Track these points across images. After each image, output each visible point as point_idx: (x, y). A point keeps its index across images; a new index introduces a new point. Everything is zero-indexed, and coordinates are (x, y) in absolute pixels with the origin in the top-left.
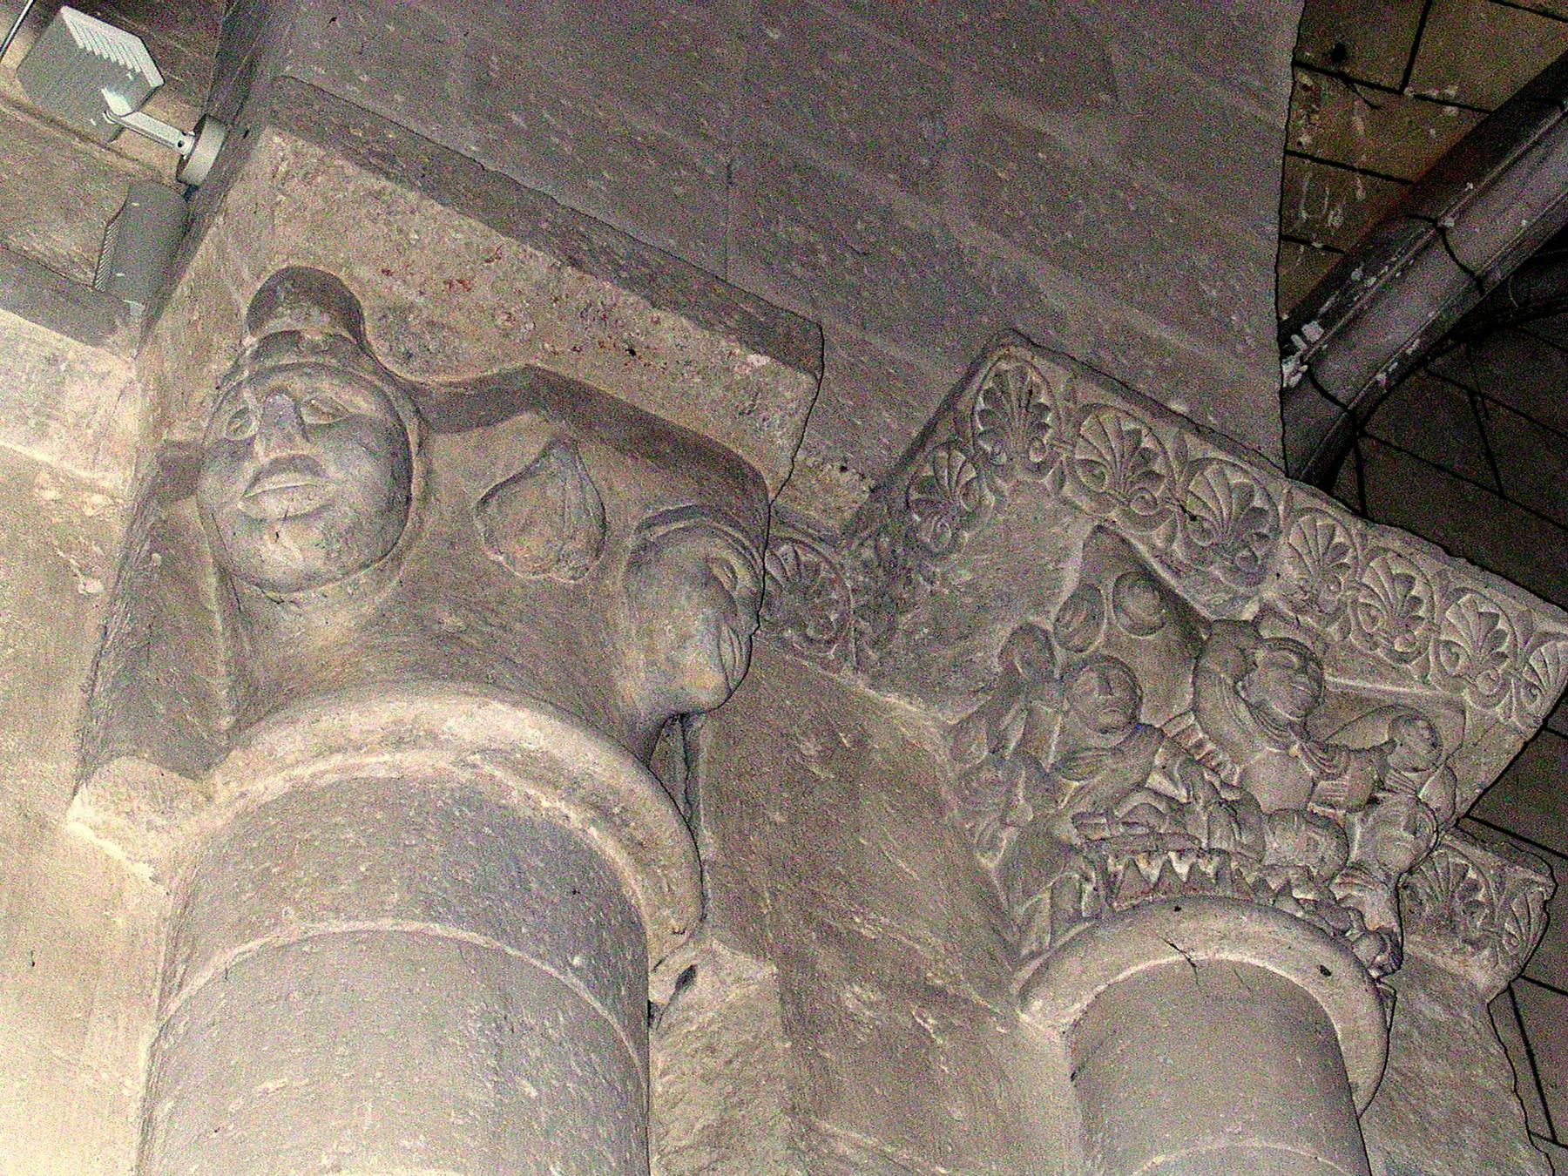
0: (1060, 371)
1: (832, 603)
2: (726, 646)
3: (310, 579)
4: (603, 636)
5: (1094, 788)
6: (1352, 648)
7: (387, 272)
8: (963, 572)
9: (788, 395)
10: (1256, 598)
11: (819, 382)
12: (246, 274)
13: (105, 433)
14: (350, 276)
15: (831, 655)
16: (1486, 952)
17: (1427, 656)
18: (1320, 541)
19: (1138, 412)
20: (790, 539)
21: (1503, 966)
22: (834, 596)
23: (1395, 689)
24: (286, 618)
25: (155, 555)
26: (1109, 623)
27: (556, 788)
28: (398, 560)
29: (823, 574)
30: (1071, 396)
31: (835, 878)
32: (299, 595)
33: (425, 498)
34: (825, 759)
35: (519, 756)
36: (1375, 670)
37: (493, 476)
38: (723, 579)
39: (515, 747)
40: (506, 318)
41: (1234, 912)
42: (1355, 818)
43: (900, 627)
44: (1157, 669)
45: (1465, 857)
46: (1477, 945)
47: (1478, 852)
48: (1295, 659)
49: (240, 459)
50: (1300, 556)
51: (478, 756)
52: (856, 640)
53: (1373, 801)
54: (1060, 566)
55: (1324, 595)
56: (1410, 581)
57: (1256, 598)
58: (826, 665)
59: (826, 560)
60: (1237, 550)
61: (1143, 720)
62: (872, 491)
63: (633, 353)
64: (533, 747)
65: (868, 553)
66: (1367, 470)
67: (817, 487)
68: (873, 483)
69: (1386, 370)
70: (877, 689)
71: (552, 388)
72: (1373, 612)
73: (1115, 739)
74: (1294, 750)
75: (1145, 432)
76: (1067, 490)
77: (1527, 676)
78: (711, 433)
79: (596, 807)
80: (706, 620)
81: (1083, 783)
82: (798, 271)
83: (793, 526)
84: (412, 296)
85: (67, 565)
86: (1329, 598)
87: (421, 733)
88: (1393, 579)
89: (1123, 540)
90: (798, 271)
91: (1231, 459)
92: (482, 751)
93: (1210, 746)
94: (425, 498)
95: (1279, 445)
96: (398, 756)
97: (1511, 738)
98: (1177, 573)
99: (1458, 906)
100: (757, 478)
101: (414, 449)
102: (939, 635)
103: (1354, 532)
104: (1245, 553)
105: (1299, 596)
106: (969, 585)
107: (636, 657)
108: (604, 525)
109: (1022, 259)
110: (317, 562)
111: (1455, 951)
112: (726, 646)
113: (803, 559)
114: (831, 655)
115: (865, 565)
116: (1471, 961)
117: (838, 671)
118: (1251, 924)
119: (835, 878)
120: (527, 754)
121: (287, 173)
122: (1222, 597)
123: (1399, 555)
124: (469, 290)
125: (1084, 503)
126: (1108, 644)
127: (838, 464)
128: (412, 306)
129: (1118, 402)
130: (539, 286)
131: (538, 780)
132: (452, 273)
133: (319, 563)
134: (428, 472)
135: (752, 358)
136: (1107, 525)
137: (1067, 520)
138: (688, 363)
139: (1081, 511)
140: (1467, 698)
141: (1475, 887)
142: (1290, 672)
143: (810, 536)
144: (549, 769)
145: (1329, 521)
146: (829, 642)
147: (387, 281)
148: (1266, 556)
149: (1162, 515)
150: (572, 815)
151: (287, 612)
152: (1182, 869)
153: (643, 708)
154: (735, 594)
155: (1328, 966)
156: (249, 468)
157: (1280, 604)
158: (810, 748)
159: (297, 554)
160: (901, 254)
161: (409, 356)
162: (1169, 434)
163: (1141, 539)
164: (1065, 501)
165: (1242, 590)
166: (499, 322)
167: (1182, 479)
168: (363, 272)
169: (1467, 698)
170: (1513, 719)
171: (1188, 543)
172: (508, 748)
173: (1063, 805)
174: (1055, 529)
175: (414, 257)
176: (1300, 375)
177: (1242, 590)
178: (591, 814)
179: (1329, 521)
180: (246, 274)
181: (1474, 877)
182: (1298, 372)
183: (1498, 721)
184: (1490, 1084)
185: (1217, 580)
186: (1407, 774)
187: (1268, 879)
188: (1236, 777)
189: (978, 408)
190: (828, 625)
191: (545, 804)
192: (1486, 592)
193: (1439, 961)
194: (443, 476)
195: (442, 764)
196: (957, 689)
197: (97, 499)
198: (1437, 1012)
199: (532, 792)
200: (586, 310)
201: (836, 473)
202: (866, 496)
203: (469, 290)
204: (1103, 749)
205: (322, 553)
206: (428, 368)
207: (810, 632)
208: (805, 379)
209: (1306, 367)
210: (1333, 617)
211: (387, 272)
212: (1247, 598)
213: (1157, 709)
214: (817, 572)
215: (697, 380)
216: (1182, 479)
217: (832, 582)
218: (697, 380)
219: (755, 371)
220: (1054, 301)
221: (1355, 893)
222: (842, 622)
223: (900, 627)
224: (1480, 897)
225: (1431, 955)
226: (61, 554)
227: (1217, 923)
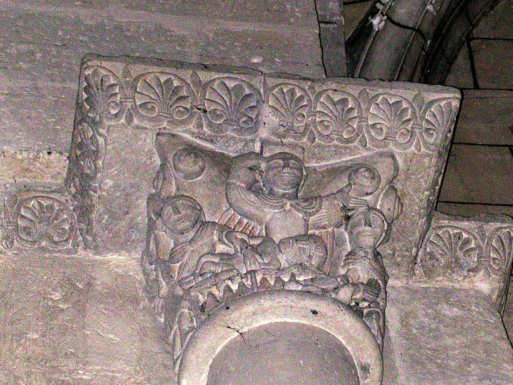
0: (118, 64)
1: (64, 221)
5: (186, 263)
6: (319, 145)
8: (108, 181)
10: (258, 139)
15: (70, 246)
16: (482, 273)
17: (363, 136)
18: (287, 99)
19: (167, 70)
20: (35, 197)
21: (494, 276)
22: (65, 216)
23: (352, 157)
26: (175, 179)
30: (127, 73)
34: (65, 299)
36: (337, 152)
41: (256, 300)
42: (342, 229)
43: (94, 219)
44: (209, 193)
45: (458, 228)
46: (475, 270)
47: (466, 223)
48: (281, 162)
50: (277, 109)
53: (348, 218)
54: (153, 160)
55: (296, 125)
56: (344, 101)
57: (258, 139)
58: (68, 252)
60: (239, 119)
61: (208, 218)
62: (68, 158)
66: (475, 57)
67: (42, 167)
68: (67, 154)
69: (431, 3)
70: (99, 254)
72: (326, 123)
73: (191, 235)
74: (288, 207)
75: (173, 78)
76: (136, 121)
77: (424, 125)
81: (180, 263)
82: (24, 66)
83: (35, 190)
86: (300, 125)
88: (334, 104)
89: (173, 135)
90: (24, 66)
91: (227, 75)
93: (245, 221)
95: (320, 60)
97: (426, 160)
98: (212, 141)
99: (460, 254)
102: (113, 216)
103: (307, 88)
104: (245, 119)
105: (282, 129)
106: (114, 186)
109: (158, 18)
111: (465, 277)
113: (45, 204)
114: (70, 246)
116: (475, 279)
117: (76, 252)
118: (266, 303)
122: (240, 145)
123: (335, 90)
125: (146, 124)
126: (178, 189)
127: (45, 152)
129: (156, 69)
136: (163, 131)
137: (143, 136)
139: (146, 128)
140: (393, 148)
141: (467, 241)
142: (280, 169)
145: (290, 87)
146: (66, 240)
148: (257, 116)
149: (192, 115)
152: (235, 287)
155: (317, 309)
157: (272, 137)
160: (85, 39)
162: (187, 74)
163: (185, 132)
164: (138, 127)
165: (249, 137)
167: (199, 95)
169: (393, 148)
170: (423, 149)
171: (210, 125)
173: (176, 277)
174: (140, 143)
176: (383, 22)
177: (249, 137)
179: (290, 87)
181: (467, 236)
182: (382, 21)
183: (414, 154)
184: (489, 338)
185: (233, 138)
186: (364, 198)
187: (282, 276)
188: (264, 231)
189: (84, 98)
192: (393, 92)
193: (457, 286)
196: (139, 240)
198: (456, 311)
201: (47, 156)
204: (184, 243)
209: (386, 17)
210: (303, 134)
212: (253, 141)
213: (214, 213)
216: (199, 95)
220: (179, 32)
221: (351, 267)
223: (94, 219)
224: (473, 245)
225: (451, 284)
227: (249, 308)
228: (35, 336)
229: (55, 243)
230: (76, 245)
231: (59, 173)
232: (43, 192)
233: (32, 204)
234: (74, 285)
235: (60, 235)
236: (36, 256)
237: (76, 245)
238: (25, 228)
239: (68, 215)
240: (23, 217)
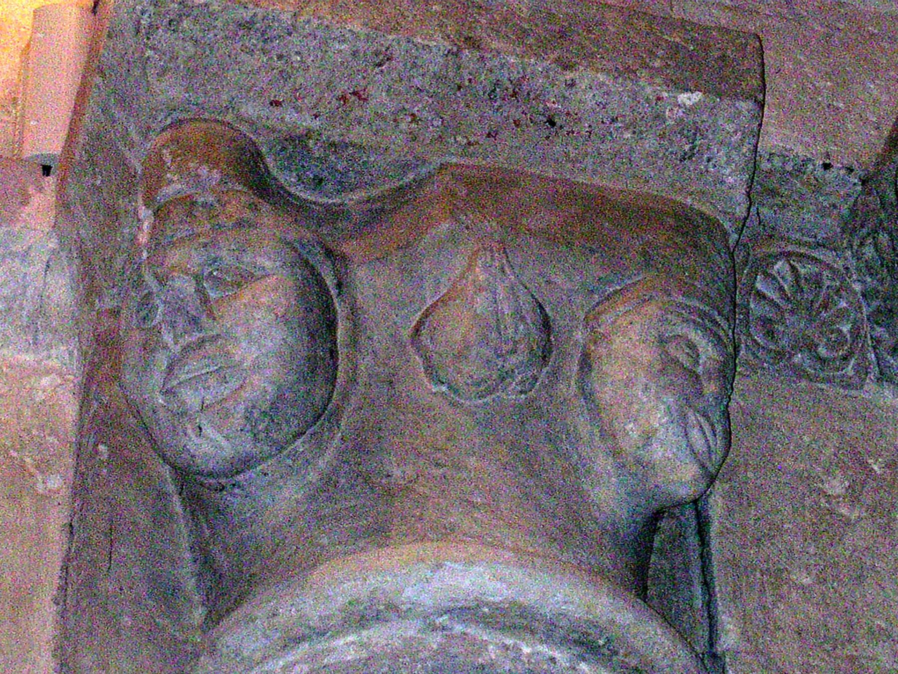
1: (842, 315)
2: (695, 434)
3: (246, 463)
4: (565, 446)
7: (276, 103)
9: (730, 128)
11: (761, 105)
12: (134, 135)
13: (40, 311)
14: (240, 118)
15: (850, 370)
22: (843, 304)
24: (235, 502)
25: (101, 448)
27: (533, 632)
28: (336, 416)
29: (827, 283)
31: (875, 634)
32: (240, 477)
33: (354, 343)
34: (853, 496)
35: (486, 610)
37: (423, 301)
38: (682, 358)
39: (480, 604)
40: (410, 120)
49: (153, 351)
51: (446, 617)
52: (874, 348)
59: (829, 267)
62: (864, 182)
63: (553, 124)
64: (498, 599)
65: (869, 252)
71: (470, 185)
78: (655, 188)
79: (579, 643)
80: (669, 412)
84: (307, 122)
85: (23, 466)
87: (382, 607)
92: (448, 611)
94: (354, 343)
96: (365, 633)
100: (712, 226)
101: (333, 292)
107: (603, 463)
108: (546, 325)
110: (247, 446)
112: (695, 434)
113: (802, 271)
114: (850, 370)
115: (869, 268)
119: (875, 634)
120: (496, 608)
121: (151, 26)
124: (365, 100)
128: (308, 133)
130: (438, 78)
131: (513, 629)
132: (343, 86)
133: (248, 447)
134: (354, 312)
135: (684, 98)
138: (614, 120)
143: (806, 244)
144: (521, 616)
146: (845, 358)
147: (277, 111)
150: (557, 655)
151: (235, 495)
153: (623, 513)
154: (700, 370)
156: (161, 361)
158: (836, 486)
159: (224, 443)
161: (319, 181)
166: (403, 126)
168: (250, 110)
172: (473, 605)
175: (301, 80)
178: (576, 650)
180: (134, 135)
190: (841, 342)
191: (526, 650)
194: (372, 309)
195: (411, 633)
197: (45, 381)
199: (509, 642)
200: (494, 91)
202: (859, 188)
203: (365, 100)
205: (250, 436)
206: (343, 187)
207: (822, 351)
208: (745, 106)
211: (276, 103)
214: (819, 284)
215: (628, 135)
217: (838, 291)
218: (628, 135)
219: (691, 110)
222: (856, 332)
226: (15, 455)
228: (806, 581)
229: (822, 360)
230: (863, 370)
231: (835, 206)
232: (800, 243)
233: (776, 267)
234: (865, 466)
235: (832, 346)
236: (242, 352)
237: (863, 370)
238: (765, 322)
239: (850, 303)
240: (761, 296)
